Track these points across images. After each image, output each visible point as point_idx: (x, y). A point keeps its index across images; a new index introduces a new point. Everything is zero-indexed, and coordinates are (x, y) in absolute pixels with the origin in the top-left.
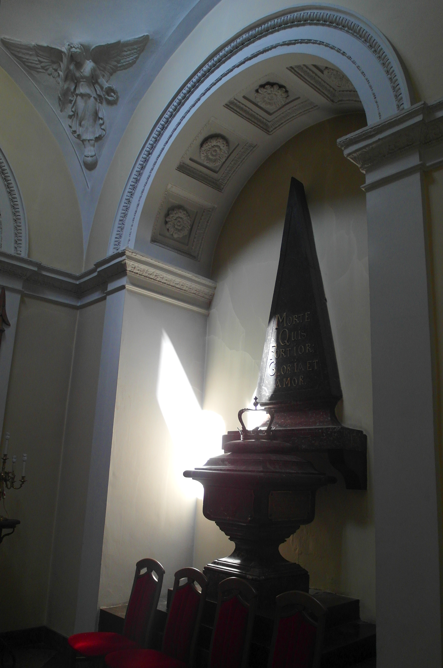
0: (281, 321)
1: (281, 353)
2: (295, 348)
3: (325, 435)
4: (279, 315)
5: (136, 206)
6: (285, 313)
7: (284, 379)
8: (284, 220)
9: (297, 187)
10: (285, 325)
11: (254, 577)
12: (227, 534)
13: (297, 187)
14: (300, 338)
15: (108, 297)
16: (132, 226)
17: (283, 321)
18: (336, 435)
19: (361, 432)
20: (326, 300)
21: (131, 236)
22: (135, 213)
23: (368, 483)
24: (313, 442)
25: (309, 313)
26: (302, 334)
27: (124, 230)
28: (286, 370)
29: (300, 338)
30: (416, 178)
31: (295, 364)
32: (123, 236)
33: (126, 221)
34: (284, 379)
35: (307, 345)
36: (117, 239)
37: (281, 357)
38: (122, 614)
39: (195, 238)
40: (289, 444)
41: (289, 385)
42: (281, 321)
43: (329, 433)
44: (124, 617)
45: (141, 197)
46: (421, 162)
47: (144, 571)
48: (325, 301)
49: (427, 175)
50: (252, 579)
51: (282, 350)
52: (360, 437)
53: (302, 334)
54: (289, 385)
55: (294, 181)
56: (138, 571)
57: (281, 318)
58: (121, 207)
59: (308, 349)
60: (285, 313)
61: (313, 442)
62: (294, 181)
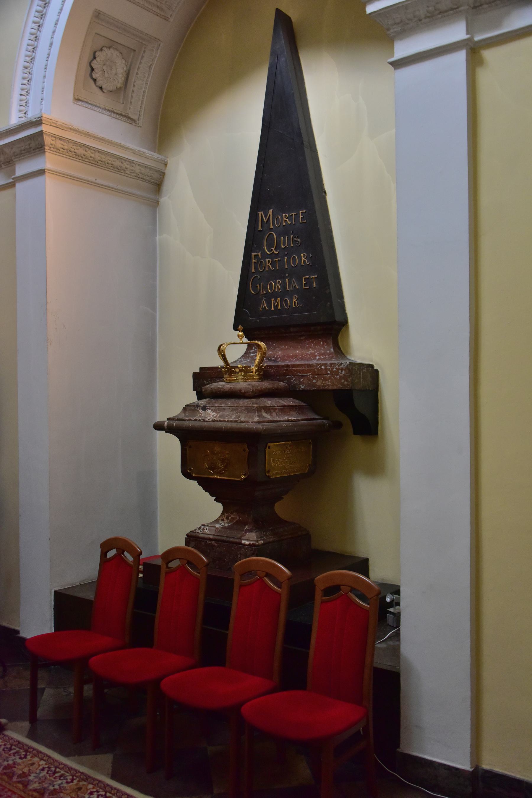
0: (265, 221)
1: (267, 264)
2: (286, 258)
3: (329, 372)
4: (262, 212)
5: (48, 47)
6: (271, 211)
7: (273, 299)
8: (267, 70)
9: (282, 20)
10: (272, 227)
11: (252, 543)
12: (212, 495)
13: (282, 20)
14: (292, 245)
15: (18, 185)
16: (45, 77)
17: (268, 220)
18: (343, 373)
19: (372, 366)
20: (325, 193)
21: (44, 92)
22: (48, 58)
23: (379, 427)
24: (315, 381)
25: (304, 211)
26: (296, 239)
27: (33, 83)
28: (275, 288)
29: (292, 245)
30: (461, 56)
31: (287, 279)
32: (32, 92)
33: (35, 68)
34: (273, 299)
35: (302, 255)
36: (22, 97)
37: (267, 269)
38: (90, 595)
39: (133, 91)
40: (283, 383)
41: (279, 307)
42: (265, 221)
43: (335, 370)
44: (93, 599)
45: (54, 32)
46: (468, 36)
47: (111, 554)
48: (324, 194)
49: (474, 51)
50: (250, 545)
51: (269, 261)
52: (371, 373)
53: (296, 239)
54: (279, 307)
55: (278, 11)
56: (104, 554)
57: (266, 216)
58: (24, 46)
59: (304, 261)
60: (271, 211)
61: (315, 381)
62: (278, 11)
